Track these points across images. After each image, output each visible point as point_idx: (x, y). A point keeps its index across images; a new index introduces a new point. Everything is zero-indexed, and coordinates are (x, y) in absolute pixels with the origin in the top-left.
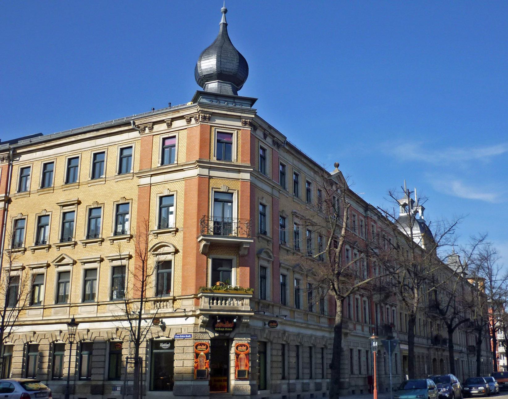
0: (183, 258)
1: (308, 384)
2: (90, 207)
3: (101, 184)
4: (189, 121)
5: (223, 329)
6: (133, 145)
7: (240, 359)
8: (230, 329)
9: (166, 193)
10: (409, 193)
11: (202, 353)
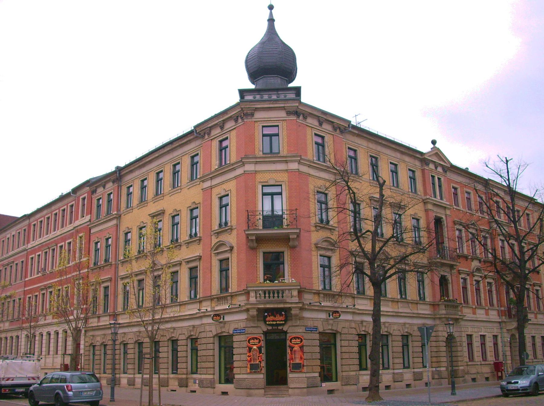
0: (237, 255)
1: (421, 373)
2: (172, 215)
3: (178, 193)
4: (236, 121)
5: (275, 323)
6: (199, 152)
7: (295, 351)
8: (282, 322)
9: (223, 194)
10: (507, 161)
11: (255, 347)
